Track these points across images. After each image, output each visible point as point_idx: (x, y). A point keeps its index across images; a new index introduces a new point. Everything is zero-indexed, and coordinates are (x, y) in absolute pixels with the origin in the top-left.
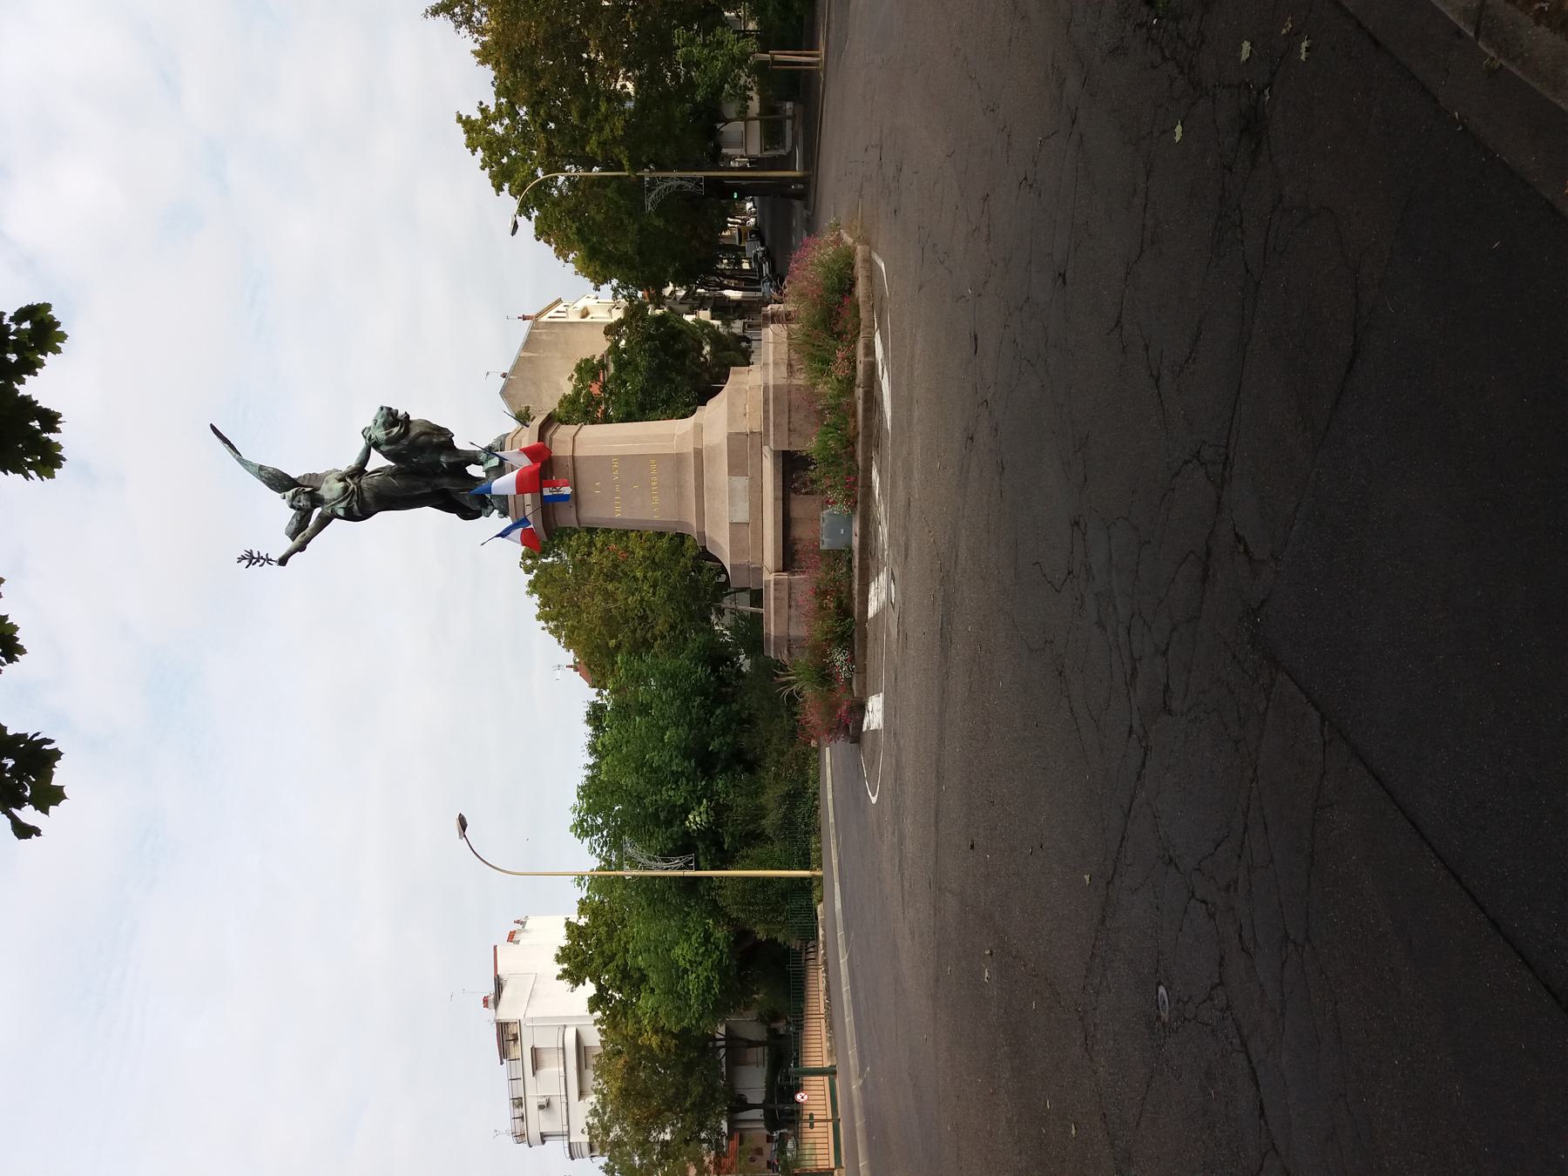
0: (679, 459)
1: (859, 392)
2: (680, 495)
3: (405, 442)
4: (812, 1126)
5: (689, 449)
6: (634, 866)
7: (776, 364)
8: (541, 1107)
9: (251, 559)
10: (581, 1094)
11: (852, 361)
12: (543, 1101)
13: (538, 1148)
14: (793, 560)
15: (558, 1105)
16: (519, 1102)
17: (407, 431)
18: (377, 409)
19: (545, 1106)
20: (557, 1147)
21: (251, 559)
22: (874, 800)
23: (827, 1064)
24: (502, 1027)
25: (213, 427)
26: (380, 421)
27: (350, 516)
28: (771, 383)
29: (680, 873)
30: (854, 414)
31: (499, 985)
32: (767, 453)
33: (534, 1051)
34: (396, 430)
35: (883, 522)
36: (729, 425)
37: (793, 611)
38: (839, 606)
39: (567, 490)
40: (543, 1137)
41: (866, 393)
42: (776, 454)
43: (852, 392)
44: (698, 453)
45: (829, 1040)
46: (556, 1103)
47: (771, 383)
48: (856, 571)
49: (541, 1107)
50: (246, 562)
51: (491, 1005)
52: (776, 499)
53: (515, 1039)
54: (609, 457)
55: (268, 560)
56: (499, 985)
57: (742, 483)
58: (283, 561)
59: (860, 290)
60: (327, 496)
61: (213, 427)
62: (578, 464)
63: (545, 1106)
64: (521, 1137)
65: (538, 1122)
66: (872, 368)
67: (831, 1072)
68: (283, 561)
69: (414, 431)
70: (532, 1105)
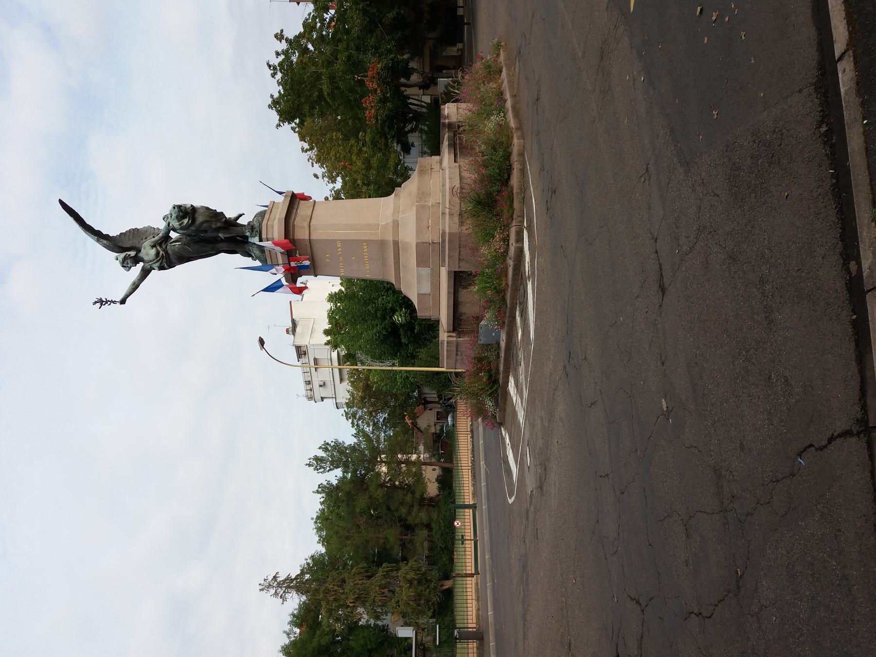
0: (382, 243)
1: (511, 263)
2: (384, 264)
3: (193, 228)
4: (463, 543)
5: (390, 238)
6: (363, 364)
7: (451, 215)
8: (320, 386)
9: (101, 302)
10: (341, 380)
11: (506, 240)
12: (322, 383)
13: (320, 403)
14: (460, 325)
15: (329, 384)
16: (308, 383)
17: (194, 220)
18: (171, 207)
19: (323, 385)
20: (329, 403)
21: (101, 302)
22: (511, 501)
23: (472, 502)
24: (298, 348)
25: (61, 202)
26: (174, 215)
27: (161, 268)
28: (447, 231)
29: (390, 368)
30: (506, 275)
31: (294, 324)
32: (444, 272)
33: (316, 360)
34: (186, 221)
35: (522, 363)
36: (417, 236)
37: (459, 357)
38: (490, 377)
39: (307, 263)
40: (322, 399)
41: (515, 265)
42: (449, 273)
43: (505, 260)
44: (396, 244)
45: (473, 485)
46: (328, 384)
47: (447, 231)
48: (502, 360)
49: (320, 386)
50: (98, 305)
51: (291, 333)
52: (449, 293)
53: (305, 354)
54: (335, 241)
55: (114, 302)
56: (294, 324)
57: (426, 271)
58: (123, 302)
59: (515, 181)
60: (146, 258)
61: (61, 202)
62: (313, 243)
63: (323, 385)
64: (310, 398)
65: (319, 392)
66: (520, 252)
67: (473, 507)
68: (123, 302)
69: (200, 219)
70: (316, 384)
